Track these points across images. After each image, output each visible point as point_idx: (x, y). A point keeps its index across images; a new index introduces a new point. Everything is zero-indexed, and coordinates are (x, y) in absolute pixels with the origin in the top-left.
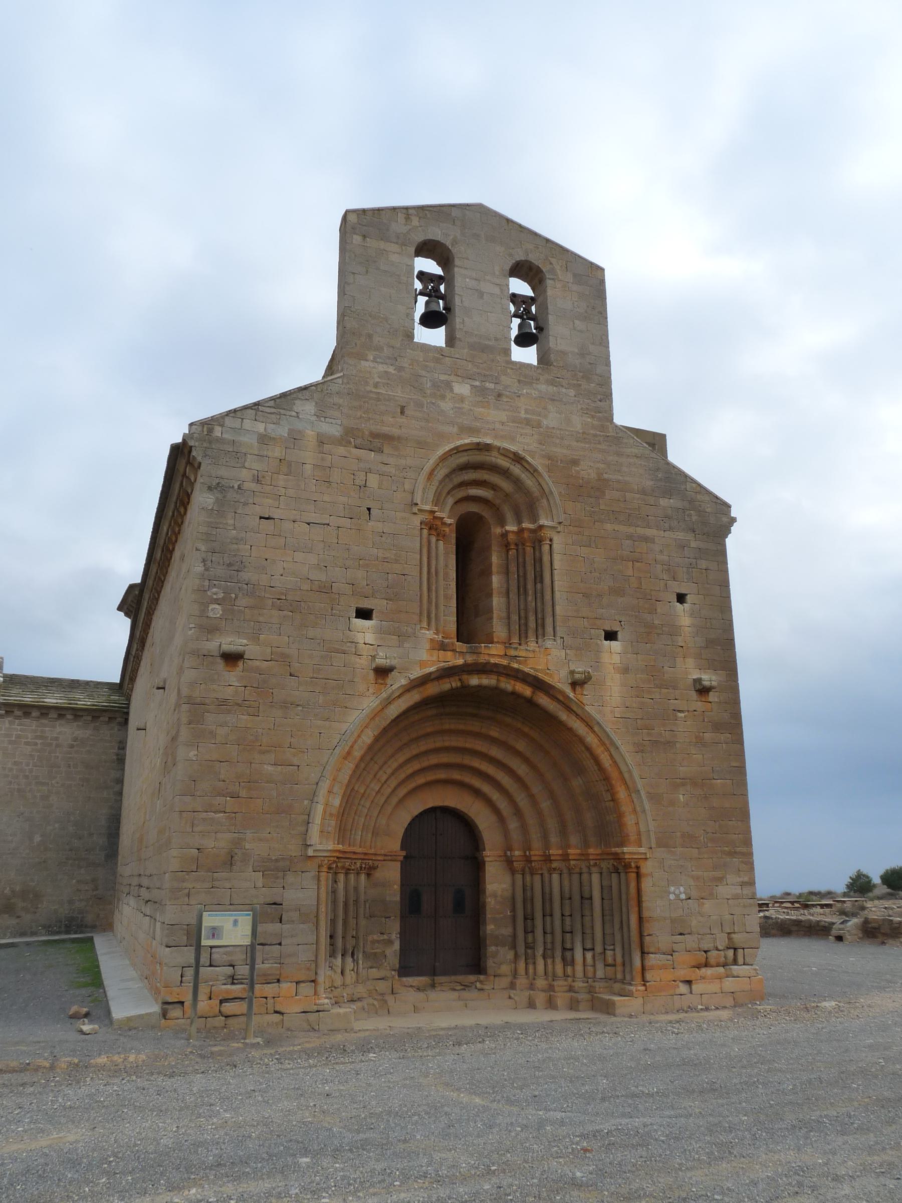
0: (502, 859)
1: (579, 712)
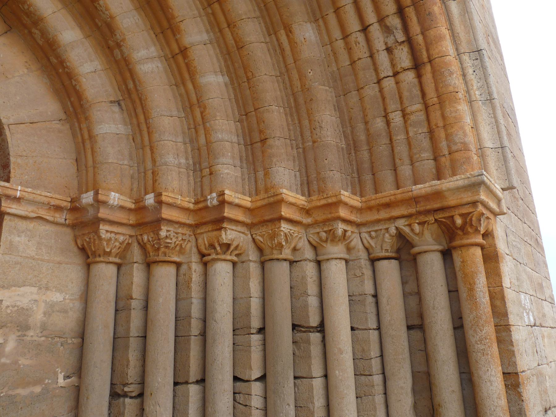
0: (60, 218)
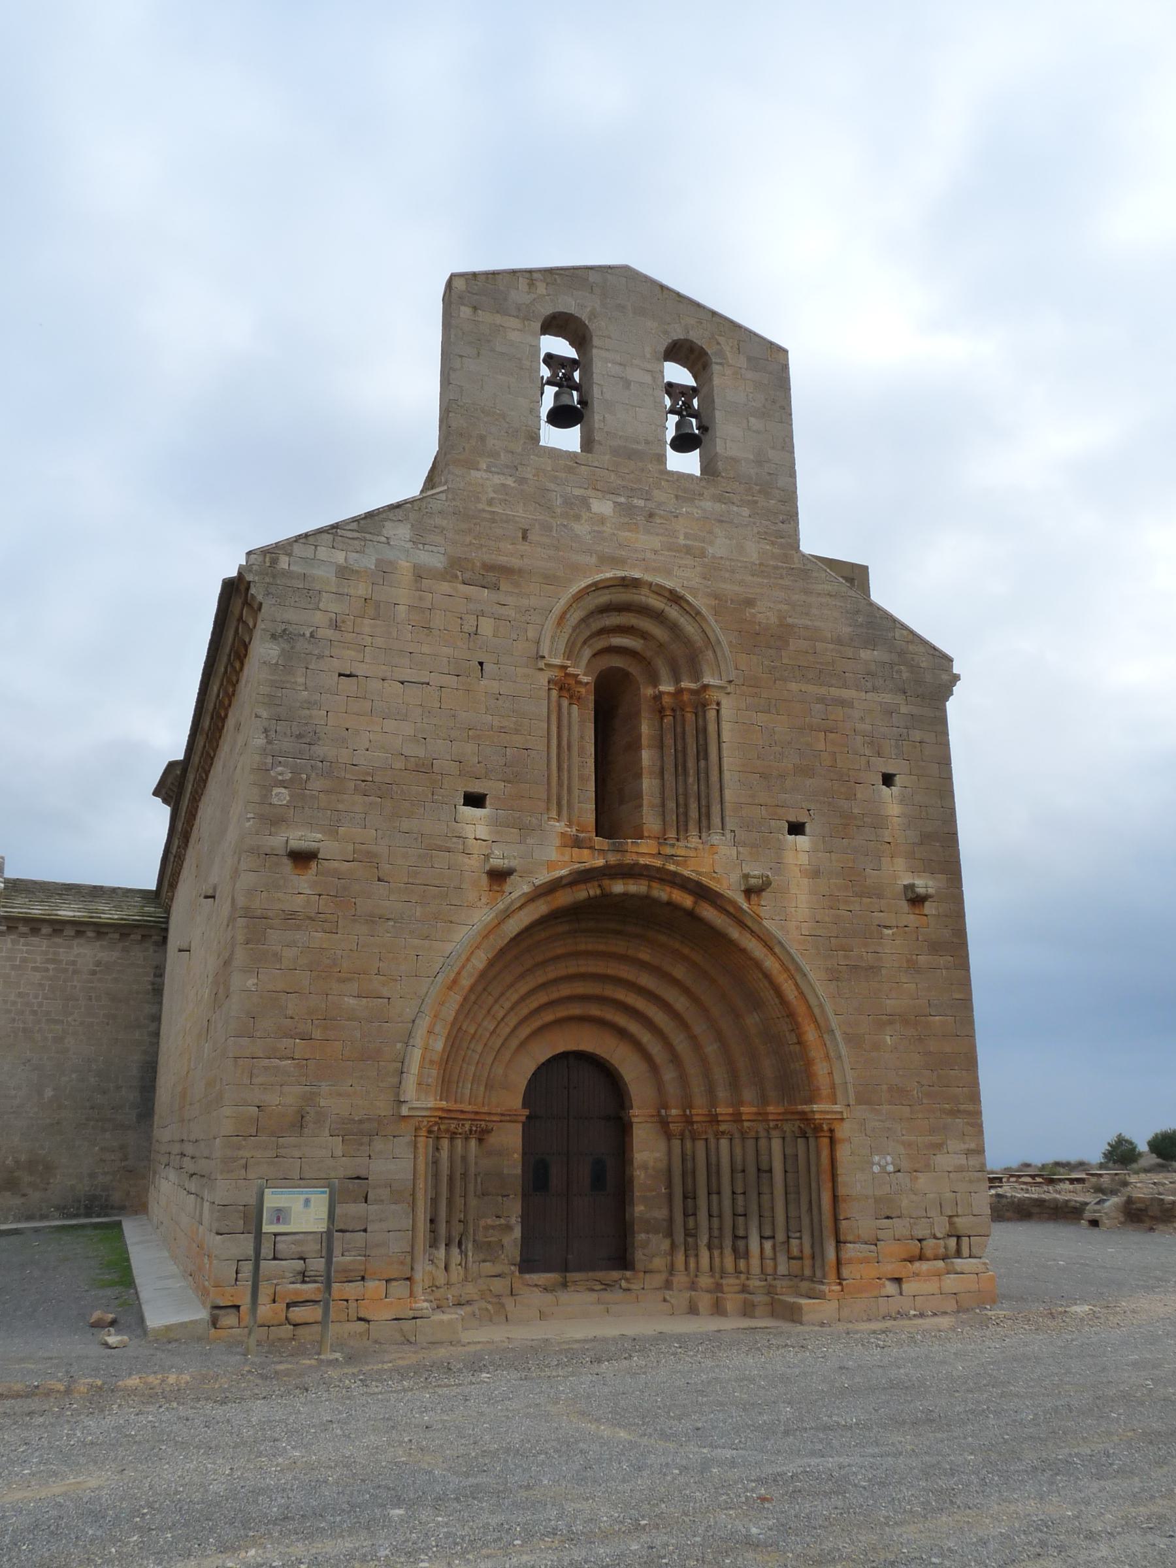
0: (654, 1119)
1: (755, 927)
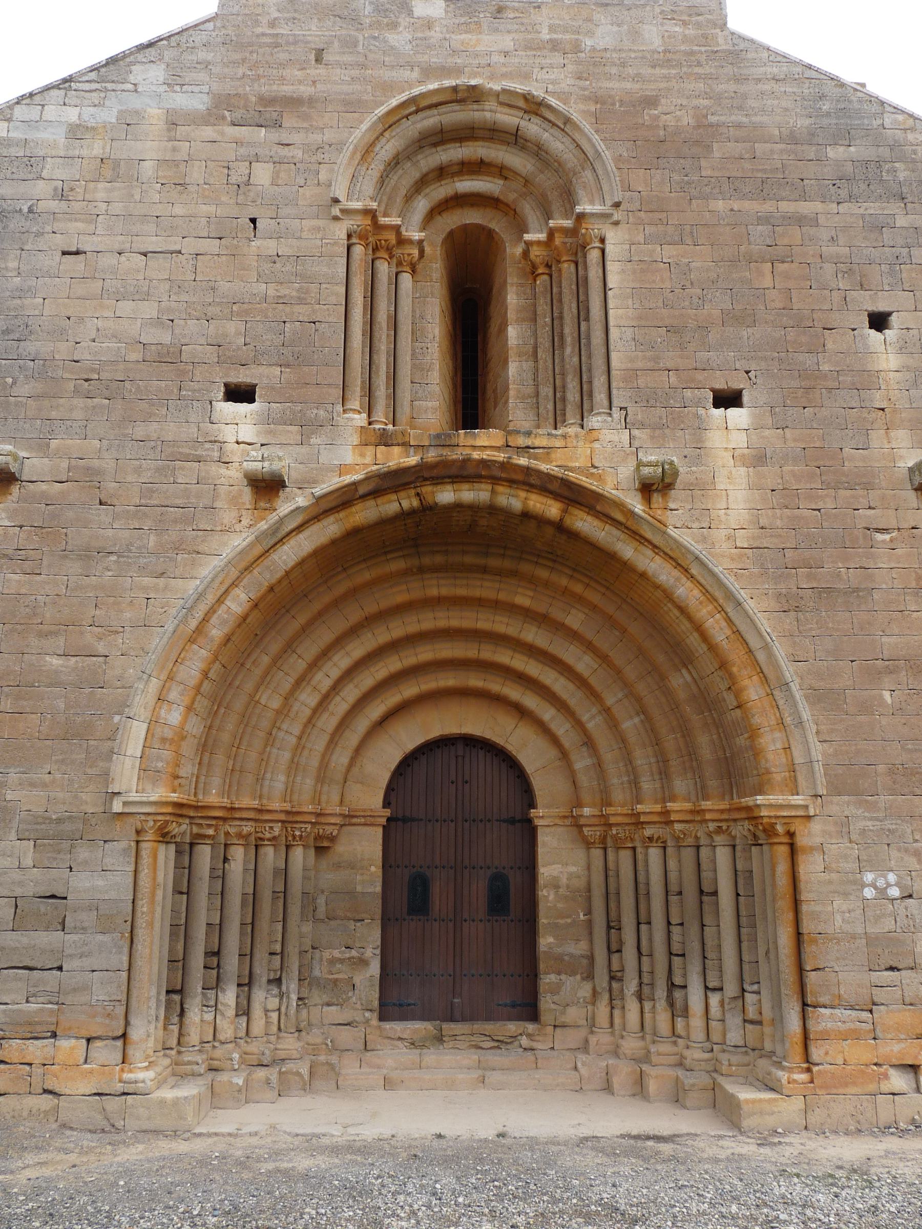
0: (568, 822)
1: (657, 540)
